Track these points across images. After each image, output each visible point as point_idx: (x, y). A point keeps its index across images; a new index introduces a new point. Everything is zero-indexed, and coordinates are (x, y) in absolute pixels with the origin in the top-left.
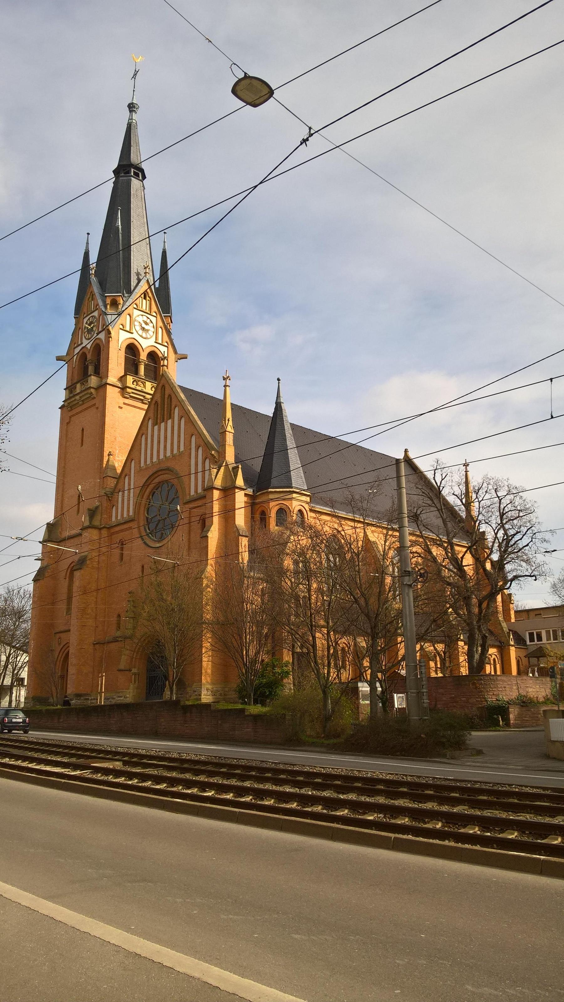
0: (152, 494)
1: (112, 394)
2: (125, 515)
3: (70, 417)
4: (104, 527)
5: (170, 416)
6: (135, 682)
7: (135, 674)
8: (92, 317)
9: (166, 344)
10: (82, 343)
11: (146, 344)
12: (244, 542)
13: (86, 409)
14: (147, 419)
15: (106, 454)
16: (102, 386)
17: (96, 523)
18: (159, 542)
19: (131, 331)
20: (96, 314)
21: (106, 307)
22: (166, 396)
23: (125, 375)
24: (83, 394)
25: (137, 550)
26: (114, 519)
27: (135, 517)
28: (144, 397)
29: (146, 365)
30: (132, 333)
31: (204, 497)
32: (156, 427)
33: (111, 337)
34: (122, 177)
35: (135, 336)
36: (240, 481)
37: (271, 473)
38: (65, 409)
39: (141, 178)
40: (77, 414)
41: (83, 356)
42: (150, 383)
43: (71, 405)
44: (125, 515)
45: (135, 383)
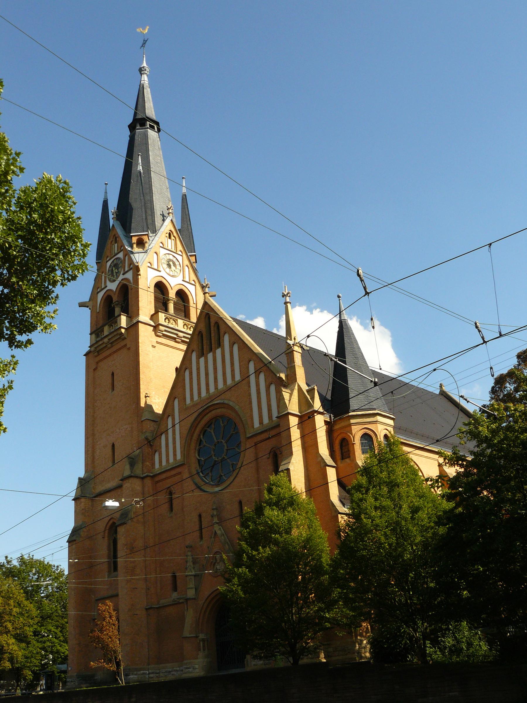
0: (202, 432)
1: (145, 334)
2: (171, 460)
3: (97, 363)
4: (147, 476)
5: (220, 344)
6: (204, 650)
7: (203, 640)
8: (117, 259)
9: (193, 283)
10: (106, 287)
11: (174, 284)
12: (332, 474)
13: (115, 352)
14: (190, 352)
15: (142, 396)
16: (133, 327)
17: (138, 470)
18: (217, 485)
19: (159, 269)
20: (121, 255)
21: (132, 247)
22: (212, 324)
23: (156, 312)
24: (113, 335)
25: (193, 498)
26: (157, 466)
27: (184, 461)
28: (177, 334)
29: (175, 304)
30: (160, 271)
31: (278, 426)
32: (202, 360)
33: (140, 275)
34: (138, 129)
35: (163, 273)
36: (317, 405)
37: (348, 394)
38: (91, 355)
39: (156, 130)
40: (105, 358)
41: (108, 299)
42: (182, 321)
43: (98, 349)
44: (171, 460)
45: (167, 321)
